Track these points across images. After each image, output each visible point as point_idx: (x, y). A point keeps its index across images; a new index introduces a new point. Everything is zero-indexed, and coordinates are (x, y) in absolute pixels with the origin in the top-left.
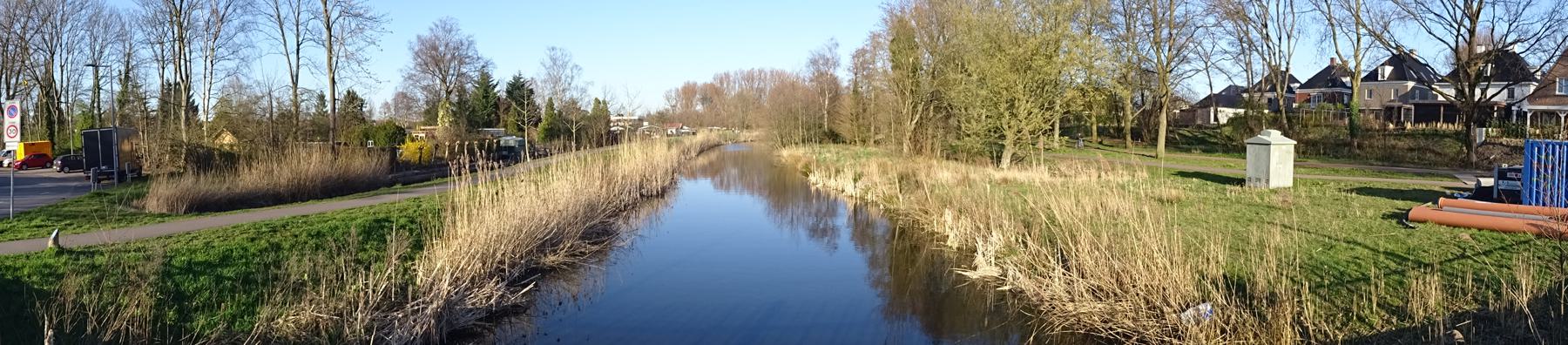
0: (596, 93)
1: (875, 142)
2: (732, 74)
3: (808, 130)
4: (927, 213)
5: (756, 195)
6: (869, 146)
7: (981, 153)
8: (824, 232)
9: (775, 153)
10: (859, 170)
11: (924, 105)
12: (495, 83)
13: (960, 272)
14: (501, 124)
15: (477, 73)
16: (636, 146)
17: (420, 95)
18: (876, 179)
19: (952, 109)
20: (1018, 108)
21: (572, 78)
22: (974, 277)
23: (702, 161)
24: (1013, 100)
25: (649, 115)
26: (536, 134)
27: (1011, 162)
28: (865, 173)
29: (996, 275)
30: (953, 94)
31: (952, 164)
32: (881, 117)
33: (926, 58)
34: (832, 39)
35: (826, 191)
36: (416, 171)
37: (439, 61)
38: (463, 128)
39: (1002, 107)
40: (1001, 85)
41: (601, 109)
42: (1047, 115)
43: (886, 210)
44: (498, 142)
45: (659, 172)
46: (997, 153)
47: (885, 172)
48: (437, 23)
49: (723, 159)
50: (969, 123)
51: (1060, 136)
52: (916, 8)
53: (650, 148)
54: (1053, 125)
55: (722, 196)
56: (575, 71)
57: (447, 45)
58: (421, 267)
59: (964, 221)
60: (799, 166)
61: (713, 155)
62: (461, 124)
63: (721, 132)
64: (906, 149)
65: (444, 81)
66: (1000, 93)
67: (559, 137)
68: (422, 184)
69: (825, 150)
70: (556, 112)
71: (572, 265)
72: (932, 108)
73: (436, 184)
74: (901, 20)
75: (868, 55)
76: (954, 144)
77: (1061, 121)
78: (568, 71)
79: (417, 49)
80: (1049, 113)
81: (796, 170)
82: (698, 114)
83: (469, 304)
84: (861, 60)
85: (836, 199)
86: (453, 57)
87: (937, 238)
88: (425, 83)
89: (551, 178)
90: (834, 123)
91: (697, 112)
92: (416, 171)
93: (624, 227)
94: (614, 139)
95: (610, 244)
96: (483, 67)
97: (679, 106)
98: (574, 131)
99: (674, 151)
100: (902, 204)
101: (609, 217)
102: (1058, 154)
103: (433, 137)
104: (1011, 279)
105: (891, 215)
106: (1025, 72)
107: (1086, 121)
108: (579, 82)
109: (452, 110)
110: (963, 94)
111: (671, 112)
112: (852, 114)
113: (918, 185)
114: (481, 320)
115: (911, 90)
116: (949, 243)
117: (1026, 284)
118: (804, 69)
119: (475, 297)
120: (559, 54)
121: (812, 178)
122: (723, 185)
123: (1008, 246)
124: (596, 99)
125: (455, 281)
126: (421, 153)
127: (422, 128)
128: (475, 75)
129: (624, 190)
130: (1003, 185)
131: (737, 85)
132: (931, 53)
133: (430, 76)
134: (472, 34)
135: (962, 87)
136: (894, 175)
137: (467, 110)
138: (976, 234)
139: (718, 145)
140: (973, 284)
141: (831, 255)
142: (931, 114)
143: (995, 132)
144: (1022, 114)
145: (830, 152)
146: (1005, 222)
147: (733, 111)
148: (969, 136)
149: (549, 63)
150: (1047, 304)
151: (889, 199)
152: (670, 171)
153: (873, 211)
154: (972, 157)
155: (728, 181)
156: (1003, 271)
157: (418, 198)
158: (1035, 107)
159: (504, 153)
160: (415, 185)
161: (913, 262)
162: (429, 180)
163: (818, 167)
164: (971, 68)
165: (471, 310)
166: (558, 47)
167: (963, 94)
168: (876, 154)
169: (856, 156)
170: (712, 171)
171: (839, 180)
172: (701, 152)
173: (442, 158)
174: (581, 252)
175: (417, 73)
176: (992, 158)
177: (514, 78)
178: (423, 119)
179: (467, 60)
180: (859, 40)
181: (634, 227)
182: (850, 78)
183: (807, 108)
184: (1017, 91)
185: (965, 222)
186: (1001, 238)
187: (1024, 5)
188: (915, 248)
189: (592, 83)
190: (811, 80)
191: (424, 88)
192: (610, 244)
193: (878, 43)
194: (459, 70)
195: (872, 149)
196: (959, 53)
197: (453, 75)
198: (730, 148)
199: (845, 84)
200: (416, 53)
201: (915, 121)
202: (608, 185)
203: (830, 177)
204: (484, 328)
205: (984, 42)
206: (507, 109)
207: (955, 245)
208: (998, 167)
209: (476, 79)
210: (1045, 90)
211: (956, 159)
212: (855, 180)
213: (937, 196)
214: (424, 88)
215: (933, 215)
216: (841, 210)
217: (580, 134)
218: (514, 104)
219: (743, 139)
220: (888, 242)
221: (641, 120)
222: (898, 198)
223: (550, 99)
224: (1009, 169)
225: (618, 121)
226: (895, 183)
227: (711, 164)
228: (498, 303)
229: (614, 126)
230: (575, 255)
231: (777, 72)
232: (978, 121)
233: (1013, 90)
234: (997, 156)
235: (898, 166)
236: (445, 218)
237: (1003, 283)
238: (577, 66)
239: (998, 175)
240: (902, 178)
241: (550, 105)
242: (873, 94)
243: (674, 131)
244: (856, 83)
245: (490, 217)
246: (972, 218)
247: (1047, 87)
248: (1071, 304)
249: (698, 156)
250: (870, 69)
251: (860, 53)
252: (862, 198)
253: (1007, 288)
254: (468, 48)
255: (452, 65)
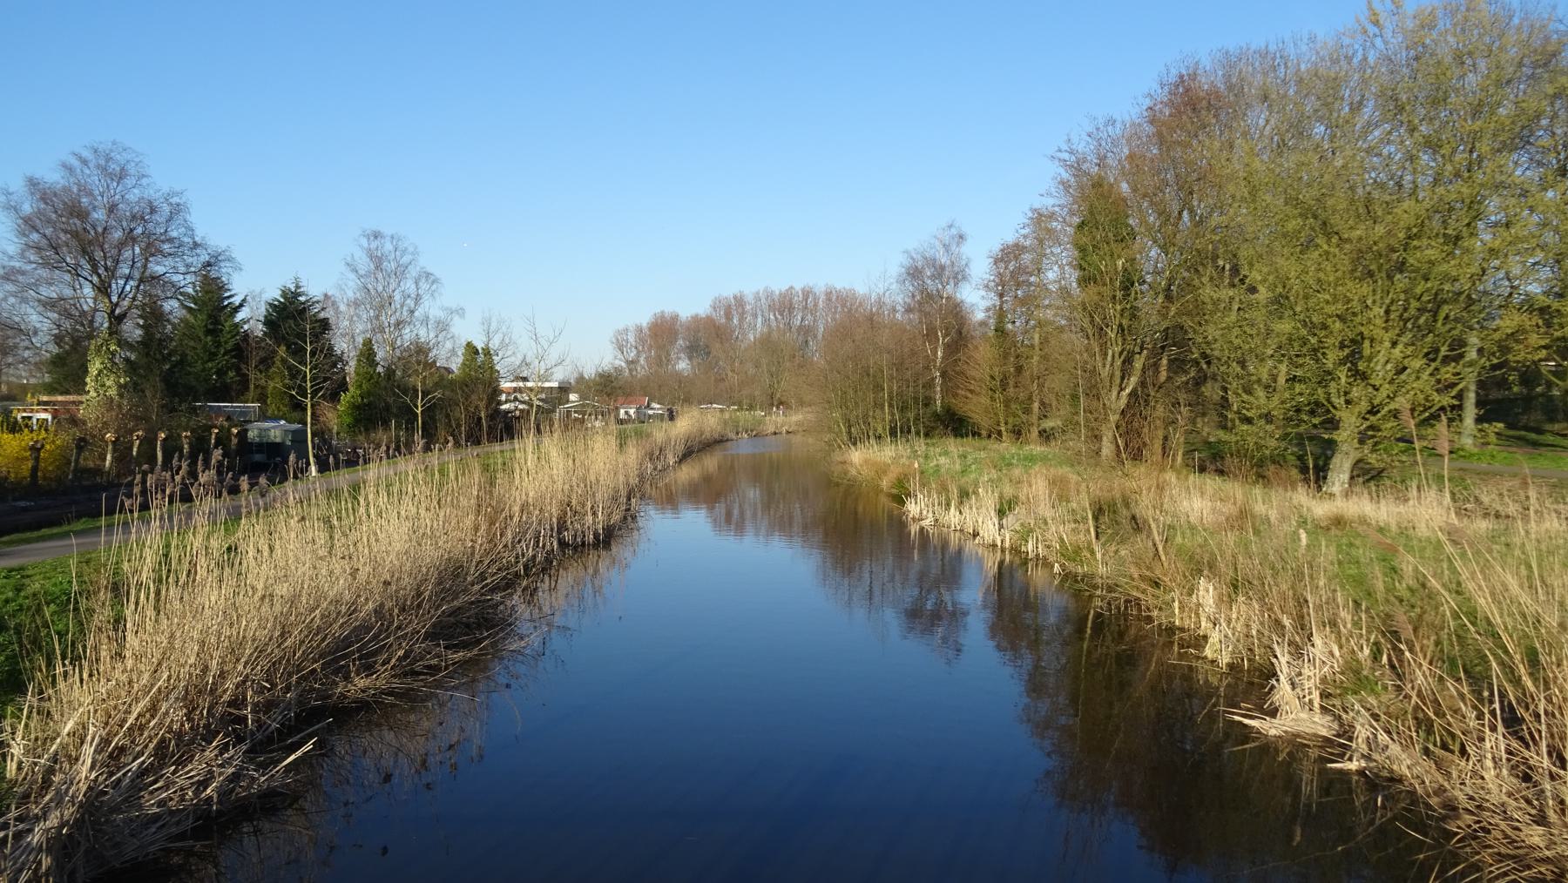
0: (468, 331)
1: (1040, 433)
2: (749, 298)
3: (903, 409)
4: (1157, 585)
5: (798, 541)
6: (1028, 443)
7: (1278, 460)
8: (936, 616)
9: (837, 456)
10: (1008, 491)
11: (1148, 358)
12: (237, 300)
13: (1237, 718)
14: (251, 393)
15: (190, 278)
16: (552, 445)
17: (41, 323)
18: (1045, 510)
19: (1209, 363)
20: (1370, 359)
21: (418, 299)
22: (1273, 732)
23: (687, 473)
24: (1357, 342)
25: (581, 379)
26: (335, 417)
27: (1352, 478)
28: (1023, 497)
29: (1324, 732)
30: (1212, 332)
31: (1211, 482)
32: (1057, 382)
33: (1151, 256)
34: (950, 227)
35: (940, 534)
36: (22, 504)
37: (90, 243)
38: (154, 399)
39: (1332, 357)
40: (1330, 309)
41: (480, 364)
42: (1447, 373)
43: (1067, 576)
44: (243, 434)
45: (599, 496)
46: (1316, 459)
47: (1063, 498)
48: (86, 154)
49: (732, 467)
50: (1249, 392)
51: (1479, 420)
52: (1131, 157)
53: (581, 445)
54: (1460, 396)
55: (729, 545)
56: (424, 286)
57: (112, 209)
58: (19, 734)
59: (1243, 608)
60: (885, 483)
61: (711, 462)
62: (148, 393)
63: (727, 415)
64: (1107, 449)
65: (103, 289)
66: (1325, 327)
67: (386, 424)
68: (35, 534)
69: (938, 450)
70: (380, 369)
71: (406, 695)
72: (1165, 361)
73: (78, 534)
74: (1098, 184)
75: (1027, 258)
76: (1212, 439)
77: (1481, 384)
78: (409, 285)
79: (27, 209)
80: (1451, 368)
81: (878, 490)
82: (679, 378)
83: (150, 805)
84: (1011, 268)
85: (960, 551)
86: (130, 238)
87: (1181, 639)
88: (50, 292)
89: (362, 510)
90: (955, 395)
91: (678, 374)
92: (22, 504)
93: (523, 610)
94: (505, 427)
95: (494, 644)
96: (209, 264)
97: (642, 361)
98: (419, 412)
99: (633, 454)
100: (1102, 564)
101: (493, 590)
102: (1475, 464)
103: (74, 421)
104: (1364, 748)
105: (1077, 586)
106: (1390, 277)
107: (1549, 385)
108: (431, 308)
109: (127, 360)
110: (1236, 331)
111: (627, 373)
112: (992, 378)
113: (1137, 525)
114: (182, 836)
115: (1120, 325)
116: (1208, 652)
117: (1405, 762)
118: (894, 286)
119: (166, 787)
120: (388, 247)
121: (913, 508)
122: (732, 522)
123: (1352, 667)
124: (469, 345)
125: (113, 757)
126: (37, 459)
127: (45, 398)
128: (188, 283)
129: (526, 533)
130: (1334, 531)
131: (760, 320)
132: (1164, 249)
133: (67, 277)
134: (178, 188)
135: (1233, 317)
136: (1082, 502)
137: (166, 359)
138: (1275, 638)
139: (720, 441)
140: (1267, 748)
141: (949, 662)
142: (1163, 375)
143: (1312, 413)
144: (1381, 369)
145: (948, 454)
146: (1343, 614)
147: (752, 371)
148: (1249, 421)
149: (365, 264)
150: (1469, 818)
151: (1075, 554)
152: (624, 493)
153: (1038, 576)
154: (1261, 469)
155: (742, 513)
156: (1341, 725)
157: (21, 569)
158: (1414, 356)
159: (258, 457)
160: (14, 537)
161: (1123, 685)
162: (58, 523)
163: (923, 485)
164: (1255, 276)
165: (156, 817)
166: (387, 230)
167: (1236, 331)
168: (1044, 459)
169: (1003, 464)
170: (708, 493)
171: (966, 510)
172: (687, 455)
173: (98, 471)
174: (429, 667)
175: (29, 267)
176: (1304, 470)
177: (284, 294)
178: (47, 378)
179: (166, 247)
180: (1009, 227)
181: (546, 609)
182: (989, 303)
183: (899, 366)
184: (1369, 321)
185: (1245, 611)
186: (1337, 653)
187: (1387, 127)
188: (1128, 660)
189: (460, 312)
190: (909, 310)
191: (49, 304)
192: (494, 644)
193: (1050, 231)
194: (145, 266)
195: (1038, 449)
196: (1226, 245)
197: (128, 278)
198: (744, 447)
199: (980, 316)
200: (27, 220)
201: (1128, 391)
202: (492, 523)
203: (948, 505)
204: (190, 853)
205: (1288, 218)
206: (266, 362)
207: (1225, 659)
208: (1319, 488)
209: (190, 290)
210: (1442, 315)
211: (1221, 472)
212: (1001, 513)
213: (1180, 551)
214: (49, 304)
215: (1171, 590)
216: (969, 574)
217: (433, 419)
218: (282, 351)
219: (771, 429)
220: (1065, 643)
221: (564, 389)
222: (1093, 553)
223: (368, 343)
224: (1347, 495)
225: (515, 390)
226: (1085, 519)
227: (707, 479)
228: (223, 793)
229: (506, 402)
230: (415, 673)
231: (839, 293)
232: (1270, 388)
233: (1358, 319)
234: (1316, 467)
235: (1088, 487)
236: (90, 611)
237: (1344, 752)
238: (428, 275)
239: (1321, 509)
240: (1100, 510)
241: (368, 354)
242: (1037, 336)
243: (632, 412)
244: (1001, 314)
245: (212, 597)
246: (1261, 600)
247: (1445, 309)
248: (1540, 830)
249: (680, 461)
250: (1030, 284)
251: (1009, 254)
252: (1015, 550)
253: (1353, 766)
254: (169, 220)
255: (127, 254)
